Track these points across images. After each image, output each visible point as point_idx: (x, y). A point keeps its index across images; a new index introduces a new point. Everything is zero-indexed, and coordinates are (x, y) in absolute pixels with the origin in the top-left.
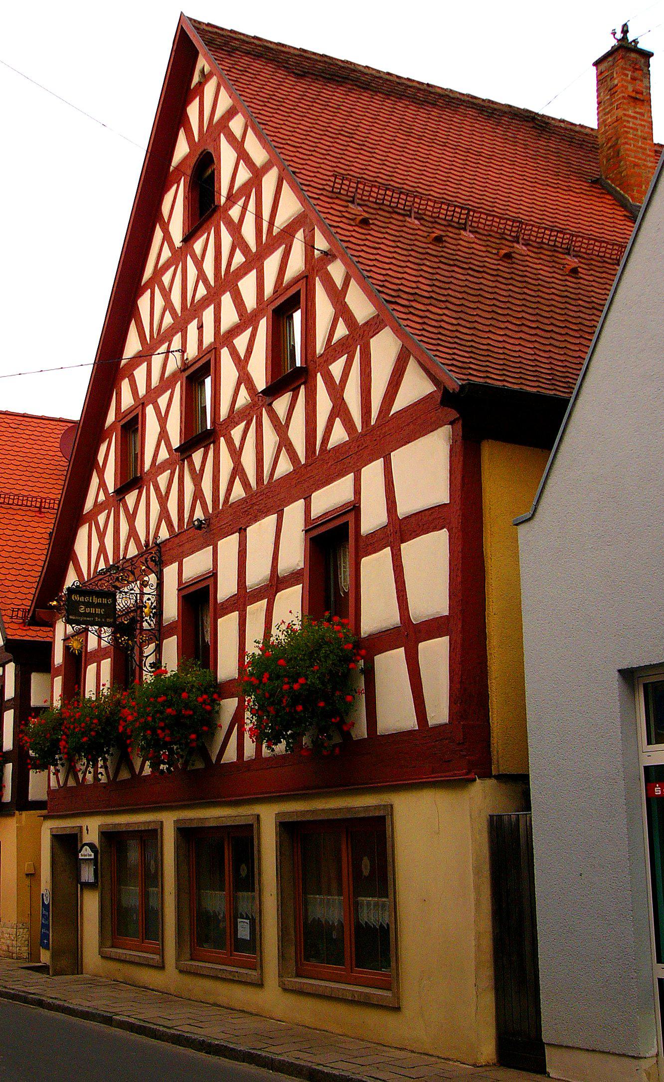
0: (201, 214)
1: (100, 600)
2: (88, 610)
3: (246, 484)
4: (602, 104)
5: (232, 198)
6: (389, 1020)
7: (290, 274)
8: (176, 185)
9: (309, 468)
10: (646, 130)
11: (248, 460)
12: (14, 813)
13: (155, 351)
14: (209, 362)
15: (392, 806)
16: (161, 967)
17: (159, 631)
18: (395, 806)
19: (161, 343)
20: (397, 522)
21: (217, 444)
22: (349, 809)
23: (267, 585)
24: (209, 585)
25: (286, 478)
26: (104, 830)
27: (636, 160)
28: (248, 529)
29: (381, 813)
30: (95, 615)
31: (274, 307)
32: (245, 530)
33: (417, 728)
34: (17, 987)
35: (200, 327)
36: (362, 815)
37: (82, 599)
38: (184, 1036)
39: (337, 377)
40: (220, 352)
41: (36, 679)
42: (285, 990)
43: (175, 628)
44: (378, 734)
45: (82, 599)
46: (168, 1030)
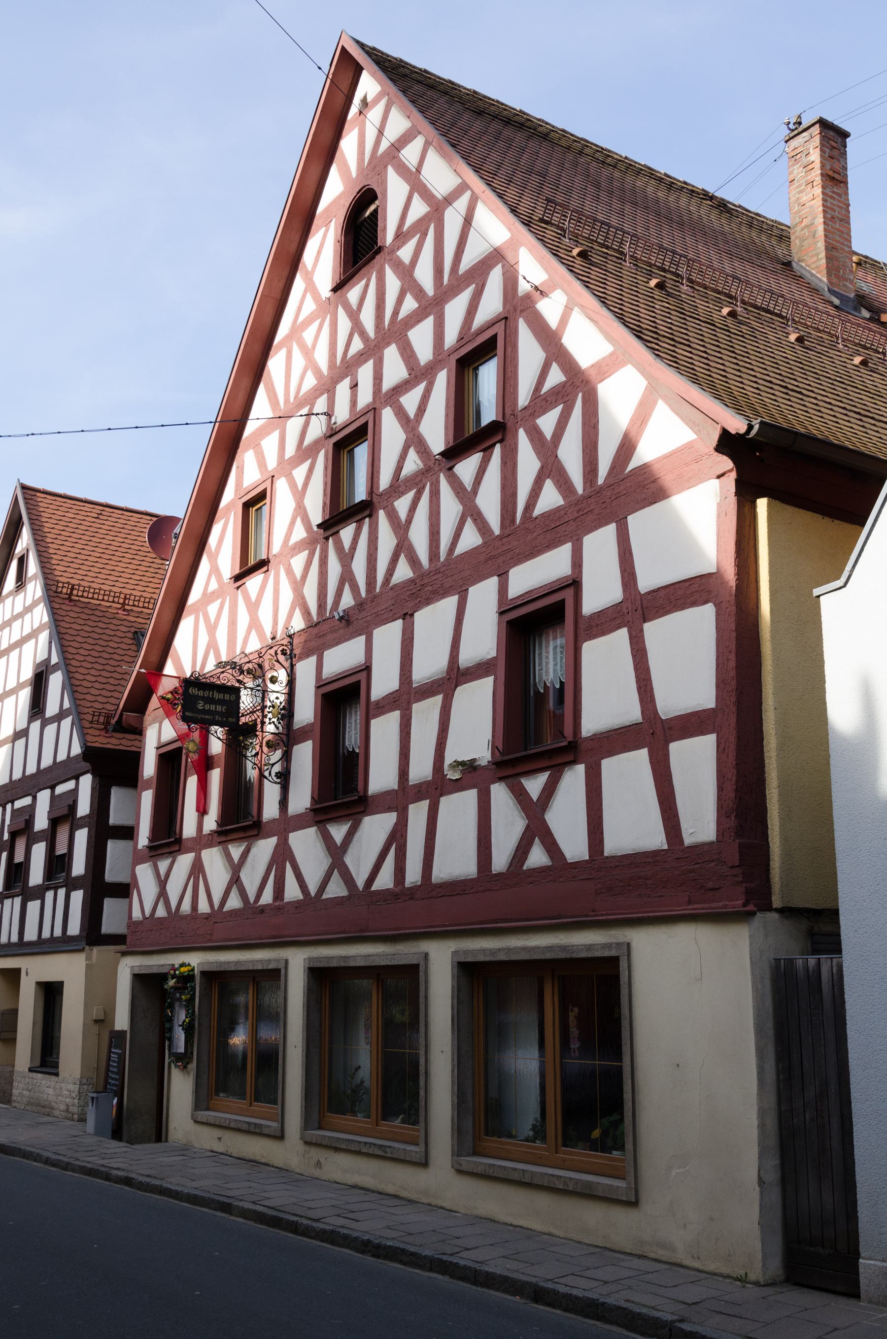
0: (355, 263)
1: (221, 696)
2: (207, 707)
3: (414, 561)
4: (795, 181)
5: (401, 237)
6: (620, 1216)
7: (482, 317)
8: (324, 229)
9: (505, 540)
10: (843, 212)
11: (419, 536)
12: (84, 948)
13: (297, 412)
14: (366, 424)
15: (629, 945)
16: (280, 1137)
17: (288, 735)
18: (634, 945)
19: (300, 406)
20: (638, 598)
21: (374, 517)
22: (563, 948)
23: (442, 679)
24: (359, 681)
25: (473, 552)
26: (205, 970)
27: (834, 243)
28: (416, 615)
29: (613, 953)
30: (214, 713)
31: (459, 357)
32: (412, 615)
33: (666, 847)
34: (94, 1161)
35: (354, 386)
36: (583, 955)
37: (201, 693)
38: (339, 1233)
39: (403, 515)
40: (381, 414)
41: (117, 795)
42: (196, 1122)
43: (311, 731)
44: (494, 872)
45: (201, 693)
46: (315, 1225)
